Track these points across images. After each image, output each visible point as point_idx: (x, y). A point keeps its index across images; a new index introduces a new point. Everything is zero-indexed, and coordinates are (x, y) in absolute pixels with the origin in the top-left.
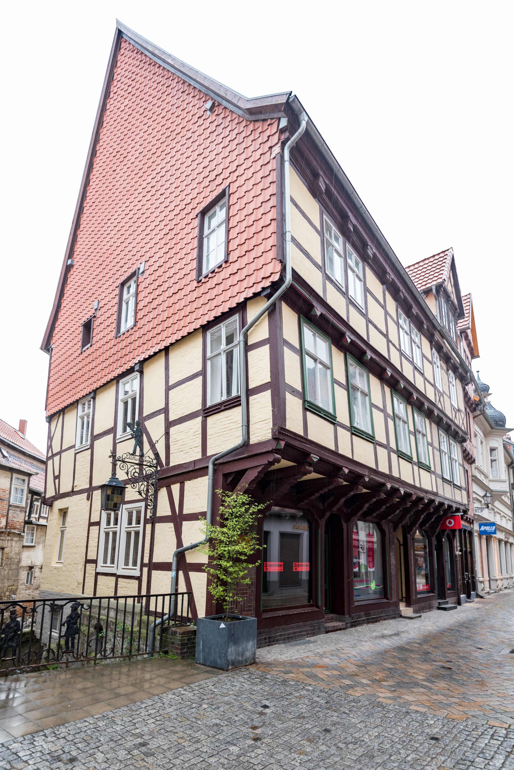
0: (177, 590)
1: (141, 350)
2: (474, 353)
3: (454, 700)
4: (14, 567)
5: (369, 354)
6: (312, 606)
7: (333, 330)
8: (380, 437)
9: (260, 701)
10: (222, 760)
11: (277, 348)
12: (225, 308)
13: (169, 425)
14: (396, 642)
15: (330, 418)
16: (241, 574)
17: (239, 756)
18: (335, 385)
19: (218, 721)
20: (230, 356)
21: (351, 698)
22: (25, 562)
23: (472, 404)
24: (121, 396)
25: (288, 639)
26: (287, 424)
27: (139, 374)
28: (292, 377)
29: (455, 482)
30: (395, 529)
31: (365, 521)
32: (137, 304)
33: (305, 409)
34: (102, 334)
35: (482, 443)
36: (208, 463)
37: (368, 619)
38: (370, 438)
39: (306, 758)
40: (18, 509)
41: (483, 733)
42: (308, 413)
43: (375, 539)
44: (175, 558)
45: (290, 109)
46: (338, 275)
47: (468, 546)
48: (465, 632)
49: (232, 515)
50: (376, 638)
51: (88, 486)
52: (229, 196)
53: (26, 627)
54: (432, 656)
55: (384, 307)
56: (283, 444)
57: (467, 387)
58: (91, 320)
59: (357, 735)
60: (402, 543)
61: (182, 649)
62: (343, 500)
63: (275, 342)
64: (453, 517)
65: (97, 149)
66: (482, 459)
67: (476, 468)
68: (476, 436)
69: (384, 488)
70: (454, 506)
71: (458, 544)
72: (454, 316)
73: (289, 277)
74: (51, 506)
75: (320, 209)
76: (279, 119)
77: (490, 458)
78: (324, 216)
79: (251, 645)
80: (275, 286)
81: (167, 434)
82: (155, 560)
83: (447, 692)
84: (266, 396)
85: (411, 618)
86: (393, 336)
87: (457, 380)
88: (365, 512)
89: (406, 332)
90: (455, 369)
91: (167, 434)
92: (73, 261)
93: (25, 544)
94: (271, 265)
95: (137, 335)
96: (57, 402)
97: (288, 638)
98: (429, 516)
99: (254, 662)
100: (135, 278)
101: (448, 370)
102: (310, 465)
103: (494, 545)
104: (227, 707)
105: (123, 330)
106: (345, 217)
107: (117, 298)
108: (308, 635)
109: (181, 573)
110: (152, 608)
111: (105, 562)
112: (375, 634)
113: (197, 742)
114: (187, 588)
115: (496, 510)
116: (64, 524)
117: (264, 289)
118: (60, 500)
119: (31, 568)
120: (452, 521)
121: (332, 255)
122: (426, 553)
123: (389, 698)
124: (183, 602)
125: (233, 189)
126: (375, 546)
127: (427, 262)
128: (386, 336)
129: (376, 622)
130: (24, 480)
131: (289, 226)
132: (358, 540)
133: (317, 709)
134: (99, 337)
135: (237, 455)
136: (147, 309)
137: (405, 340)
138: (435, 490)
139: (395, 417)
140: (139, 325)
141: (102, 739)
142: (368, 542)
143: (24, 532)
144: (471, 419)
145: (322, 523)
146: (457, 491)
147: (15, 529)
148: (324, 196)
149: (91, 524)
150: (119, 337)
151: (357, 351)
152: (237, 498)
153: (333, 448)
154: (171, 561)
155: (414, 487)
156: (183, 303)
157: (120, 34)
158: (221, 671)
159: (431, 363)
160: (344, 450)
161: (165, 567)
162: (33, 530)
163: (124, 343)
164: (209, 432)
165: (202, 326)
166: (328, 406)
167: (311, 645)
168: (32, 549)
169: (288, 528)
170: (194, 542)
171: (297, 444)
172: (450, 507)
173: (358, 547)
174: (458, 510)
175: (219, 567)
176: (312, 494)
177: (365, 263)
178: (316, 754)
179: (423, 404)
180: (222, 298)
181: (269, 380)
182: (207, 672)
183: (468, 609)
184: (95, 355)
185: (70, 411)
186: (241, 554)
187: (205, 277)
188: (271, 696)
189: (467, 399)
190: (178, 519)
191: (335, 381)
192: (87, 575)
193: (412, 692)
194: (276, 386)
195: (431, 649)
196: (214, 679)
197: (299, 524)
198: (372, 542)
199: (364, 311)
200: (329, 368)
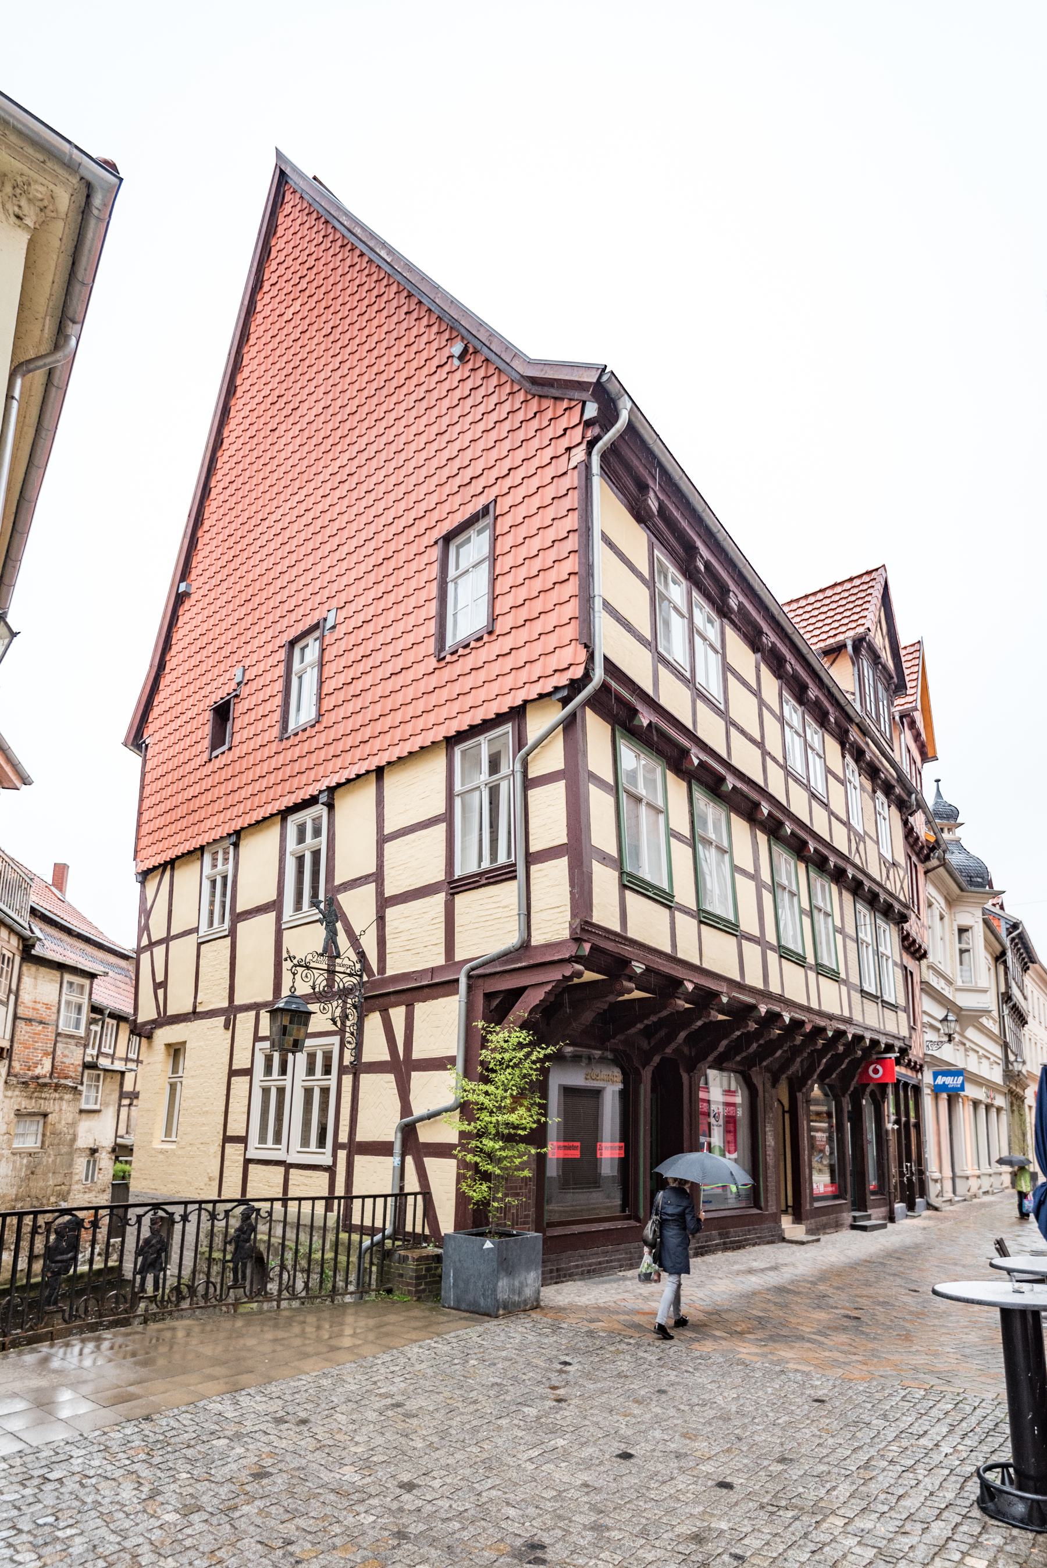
0: (402, 1188)
1: (330, 766)
2: (926, 753)
3: (855, 1358)
4: (64, 1149)
5: (731, 782)
6: (628, 1218)
7: (671, 747)
8: (749, 924)
9: (556, 1357)
10: (516, 1422)
11: (578, 788)
12: (489, 712)
13: (384, 903)
14: (773, 1279)
15: (664, 899)
16: (517, 1161)
17: (538, 1418)
18: (672, 840)
19: (499, 1381)
20: (494, 792)
21: (697, 1354)
22: (84, 1142)
23: (922, 848)
24: (291, 844)
25: (590, 1273)
26: (595, 913)
27: (325, 809)
28: (602, 834)
29: (886, 998)
30: (775, 1082)
31: (721, 1069)
32: (321, 683)
33: (624, 887)
34: (252, 730)
35: (942, 918)
36: (459, 972)
37: (725, 1243)
38: (730, 928)
39: (634, 1420)
40: (73, 1041)
41: (890, 1395)
42: (628, 893)
43: (738, 1099)
44: (399, 1135)
45: (604, 392)
46: (677, 652)
47: (912, 1114)
48: (894, 1266)
49: (501, 1064)
50: (738, 1273)
51: (226, 1004)
52: (496, 518)
53: (36, 1276)
54: (831, 1301)
55: (757, 693)
56: (587, 947)
57: (911, 819)
58: (229, 701)
59: (706, 1396)
60: (786, 1108)
61: (418, 1285)
62: (683, 1035)
63: (574, 776)
64: (881, 1061)
65: (238, 382)
66: (940, 945)
67: (930, 967)
68: (930, 905)
69: (754, 1014)
70: (883, 1040)
71: (892, 1110)
72: (887, 690)
73: (599, 674)
74: (150, 1037)
75: (649, 540)
76: (584, 403)
77: (957, 946)
78: (656, 552)
79: (532, 1278)
80: (576, 686)
81: (381, 919)
82: (359, 1138)
83: (847, 1348)
84: (560, 866)
85: (802, 1243)
86: (773, 745)
87: (893, 807)
88: (721, 1054)
89: (796, 732)
90: (888, 789)
91: (381, 919)
92: (189, 585)
93: (84, 1107)
94: (570, 650)
95: (323, 738)
96: (161, 846)
97: (589, 1272)
98: (837, 1059)
99: (536, 1306)
100: (317, 634)
101: (874, 792)
102: (630, 979)
103: (964, 1113)
104: (508, 1363)
105: (292, 726)
106: (691, 550)
107: (282, 667)
108: (621, 1267)
109: (409, 1159)
110: (356, 1220)
111: (263, 1139)
112: (736, 1267)
113: (475, 1402)
114: (421, 1186)
115: (968, 1044)
116: (175, 1070)
117: (557, 689)
118: (167, 1028)
119: (94, 1151)
120: (879, 1067)
121: (669, 614)
122: (831, 1126)
123: (756, 1354)
124: (414, 1210)
125: (503, 506)
126: (740, 1113)
127: (839, 589)
128: (760, 745)
129: (739, 1248)
130: (82, 987)
131: (601, 588)
132: (708, 1102)
133: (646, 1366)
134: (245, 734)
135: (506, 963)
136: (341, 696)
137: (795, 745)
138: (846, 1014)
139: (775, 887)
140: (326, 721)
141: (333, 1398)
142: (727, 1104)
143: (82, 1084)
144: (921, 875)
145: (647, 1074)
146: (889, 1014)
147: (66, 1078)
148: (658, 520)
149: (232, 1073)
150: (288, 738)
151: (709, 778)
152: (507, 1038)
153: (668, 949)
154: (391, 1138)
155: (809, 1010)
156: (410, 693)
157: (282, 178)
158: (487, 1318)
159: (842, 782)
160: (687, 952)
161: (382, 1149)
162: (98, 1080)
163: (297, 752)
164: (459, 920)
165: (447, 739)
166: (661, 880)
167: (628, 1283)
168: (96, 1115)
169: (576, 1078)
170: (434, 1108)
171: (609, 946)
172: (875, 1043)
173: (709, 1115)
174: (889, 1048)
175: (479, 1151)
176: (633, 1025)
177: (725, 621)
178: (648, 1416)
179: (825, 860)
180: (482, 694)
181: (564, 840)
182: (465, 1319)
183: (908, 1229)
184: (237, 767)
185: (186, 864)
186: (516, 1127)
187: (452, 654)
188: (575, 1350)
189: (911, 840)
190: (402, 1067)
191: (671, 833)
192: (226, 1163)
193: (792, 1348)
194: (576, 850)
195: (830, 1291)
196: (478, 1328)
197: (597, 1071)
198: (734, 1105)
199: (722, 707)
200: (659, 811)
